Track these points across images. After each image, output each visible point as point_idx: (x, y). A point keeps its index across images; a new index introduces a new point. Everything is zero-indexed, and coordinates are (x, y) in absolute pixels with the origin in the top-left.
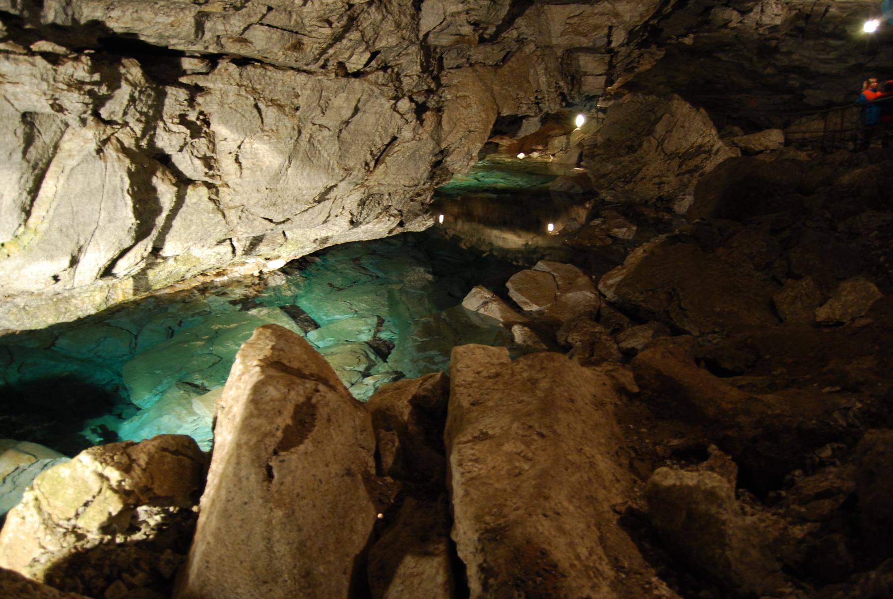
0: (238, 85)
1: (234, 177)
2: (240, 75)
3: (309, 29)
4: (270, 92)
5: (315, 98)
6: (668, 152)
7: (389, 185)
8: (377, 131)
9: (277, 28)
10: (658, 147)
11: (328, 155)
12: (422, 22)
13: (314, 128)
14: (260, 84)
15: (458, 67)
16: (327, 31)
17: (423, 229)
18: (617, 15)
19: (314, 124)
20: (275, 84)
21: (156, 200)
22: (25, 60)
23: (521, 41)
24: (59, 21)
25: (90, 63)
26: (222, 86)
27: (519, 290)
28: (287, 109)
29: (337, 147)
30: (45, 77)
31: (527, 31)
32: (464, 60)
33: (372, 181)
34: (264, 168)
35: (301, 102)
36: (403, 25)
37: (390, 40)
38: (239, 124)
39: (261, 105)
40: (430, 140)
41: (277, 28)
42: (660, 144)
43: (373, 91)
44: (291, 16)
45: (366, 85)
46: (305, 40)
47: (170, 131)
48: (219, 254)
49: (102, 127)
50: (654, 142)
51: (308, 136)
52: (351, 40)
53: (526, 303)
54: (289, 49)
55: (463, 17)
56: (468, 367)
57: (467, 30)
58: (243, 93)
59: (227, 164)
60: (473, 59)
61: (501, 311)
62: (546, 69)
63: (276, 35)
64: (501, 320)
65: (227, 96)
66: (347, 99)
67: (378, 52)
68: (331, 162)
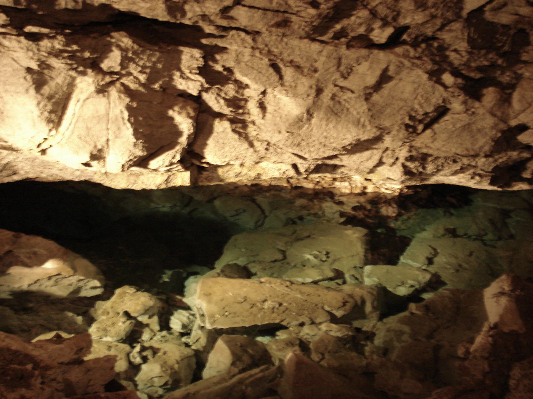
3: (296, 9)
5: (332, 64)
8: (416, 98)
9: (259, 8)
11: (358, 113)
14: (277, 48)
16: (312, 11)
19: (336, 86)
21: (175, 127)
22: (15, 39)
24: (69, 7)
25: (64, 40)
28: (306, 71)
30: (30, 48)
34: (284, 116)
35: (318, 65)
37: (416, 18)
39: (281, 65)
40: (488, 116)
41: (259, 8)
43: (402, 63)
45: (392, 57)
46: (294, 18)
47: (188, 78)
49: (100, 77)
51: (330, 95)
54: (272, 26)
56: (302, 325)
59: (252, 107)
65: (243, 55)
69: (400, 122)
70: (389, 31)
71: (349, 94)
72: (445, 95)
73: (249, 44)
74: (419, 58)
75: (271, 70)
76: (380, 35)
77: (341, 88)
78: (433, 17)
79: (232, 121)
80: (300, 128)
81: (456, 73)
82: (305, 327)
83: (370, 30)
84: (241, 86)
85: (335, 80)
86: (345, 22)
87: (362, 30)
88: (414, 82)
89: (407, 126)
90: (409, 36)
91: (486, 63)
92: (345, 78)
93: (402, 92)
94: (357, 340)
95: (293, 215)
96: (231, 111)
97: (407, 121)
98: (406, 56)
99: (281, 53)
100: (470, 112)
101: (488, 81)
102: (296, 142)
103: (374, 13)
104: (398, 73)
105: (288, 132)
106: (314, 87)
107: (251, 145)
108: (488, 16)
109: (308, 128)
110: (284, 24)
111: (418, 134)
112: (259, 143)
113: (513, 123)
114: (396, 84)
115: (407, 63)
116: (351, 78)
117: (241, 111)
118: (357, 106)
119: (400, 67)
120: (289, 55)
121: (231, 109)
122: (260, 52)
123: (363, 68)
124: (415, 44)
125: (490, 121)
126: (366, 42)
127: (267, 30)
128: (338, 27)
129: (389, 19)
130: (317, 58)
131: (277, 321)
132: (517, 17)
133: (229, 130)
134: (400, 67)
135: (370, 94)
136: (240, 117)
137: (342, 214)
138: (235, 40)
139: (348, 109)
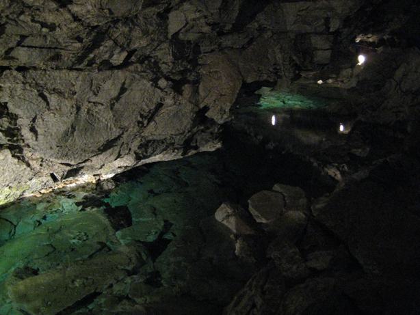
0: (23, 83)
1: (31, 141)
2: (23, 76)
3: (64, 45)
4: (52, 84)
5: (86, 86)
6: (404, 90)
7: (160, 135)
10: (396, 87)
11: (106, 120)
12: (170, 26)
13: (90, 105)
14: (42, 80)
15: (212, 51)
16: (78, 45)
17: (214, 149)
18: (332, 9)
19: (90, 102)
20: (55, 79)
23: (261, 30)
26: (9, 85)
27: (256, 207)
28: (66, 95)
29: (111, 114)
31: (266, 22)
32: (216, 46)
33: (146, 133)
34: (53, 134)
35: (77, 89)
36: (150, 31)
37: (142, 42)
38: (29, 107)
39: (46, 94)
40: (188, 104)
41: (36, 47)
42: (399, 84)
43: (134, 77)
44: (46, 39)
45: (127, 74)
46: (63, 52)
48: (43, 182)
50: (394, 83)
51: (86, 110)
52: (106, 47)
53: (258, 217)
55: (202, 21)
56: (111, 286)
57: (206, 29)
58: (28, 88)
59: (26, 133)
60: (224, 44)
61: (237, 224)
62: (281, 49)
63: (36, 52)
64: (235, 231)
65: (16, 91)
66: (113, 84)
67: (135, 50)
68: (109, 125)
69: (134, 120)
70: (125, 54)
71: (100, 107)
72: (162, 95)
73: (20, 80)
74: (144, 72)
75: (40, 99)
76: (118, 58)
77: (94, 103)
78: (153, 40)
79: (11, 148)
80: (66, 141)
81: (167, 79)
82: (114, 286)
83: (111, 56)
84: (14, 118)
85: (88, 98)
86: (96, 51)
87: (106, 56)
88: (141, 90)
89: (139, 122)
90: (136, 56)
91: (182, 69)
92: (96, 95)
93: (134, 99)
94: (153, 280)
95: (37, 218)
96: (9, 140)
97: (139, 119)
98: (136, 71)
99: (46, 84)
100: (177, 104)
101: (184, 81)
102: (65, 153)
103: (116, 42)
104: (130, 86)
105: (58, 146)
106: (74, 106)
107: (28, 165)
108: (181, 36)
109: (72, 140)
110: (57, 57)
111: (145, 127)
112: (35, 162)
113: (202, 106)
114: (129, 94)
115: (137, 76)
116: (100, 94)
117: (15, 139)
118: (105, 115)
119: (133, 80)
120: (52, 84)
121: (8, 138)
122: (30, 86)
123: (107, 85)
124: (141, 62)
125: (189, 107)
126: (107, 65)
127: (44, 64)
128: (92, 56)
129: (125, 46)
130: (74, 83)
131: (93, 291)
132: (200, 34)
133: (10, 156)
134: (133, 80)
135: (113, 104)
136: (15, 144)
137: (78, 204)
138: (8, 78)
139: (98, 119)
